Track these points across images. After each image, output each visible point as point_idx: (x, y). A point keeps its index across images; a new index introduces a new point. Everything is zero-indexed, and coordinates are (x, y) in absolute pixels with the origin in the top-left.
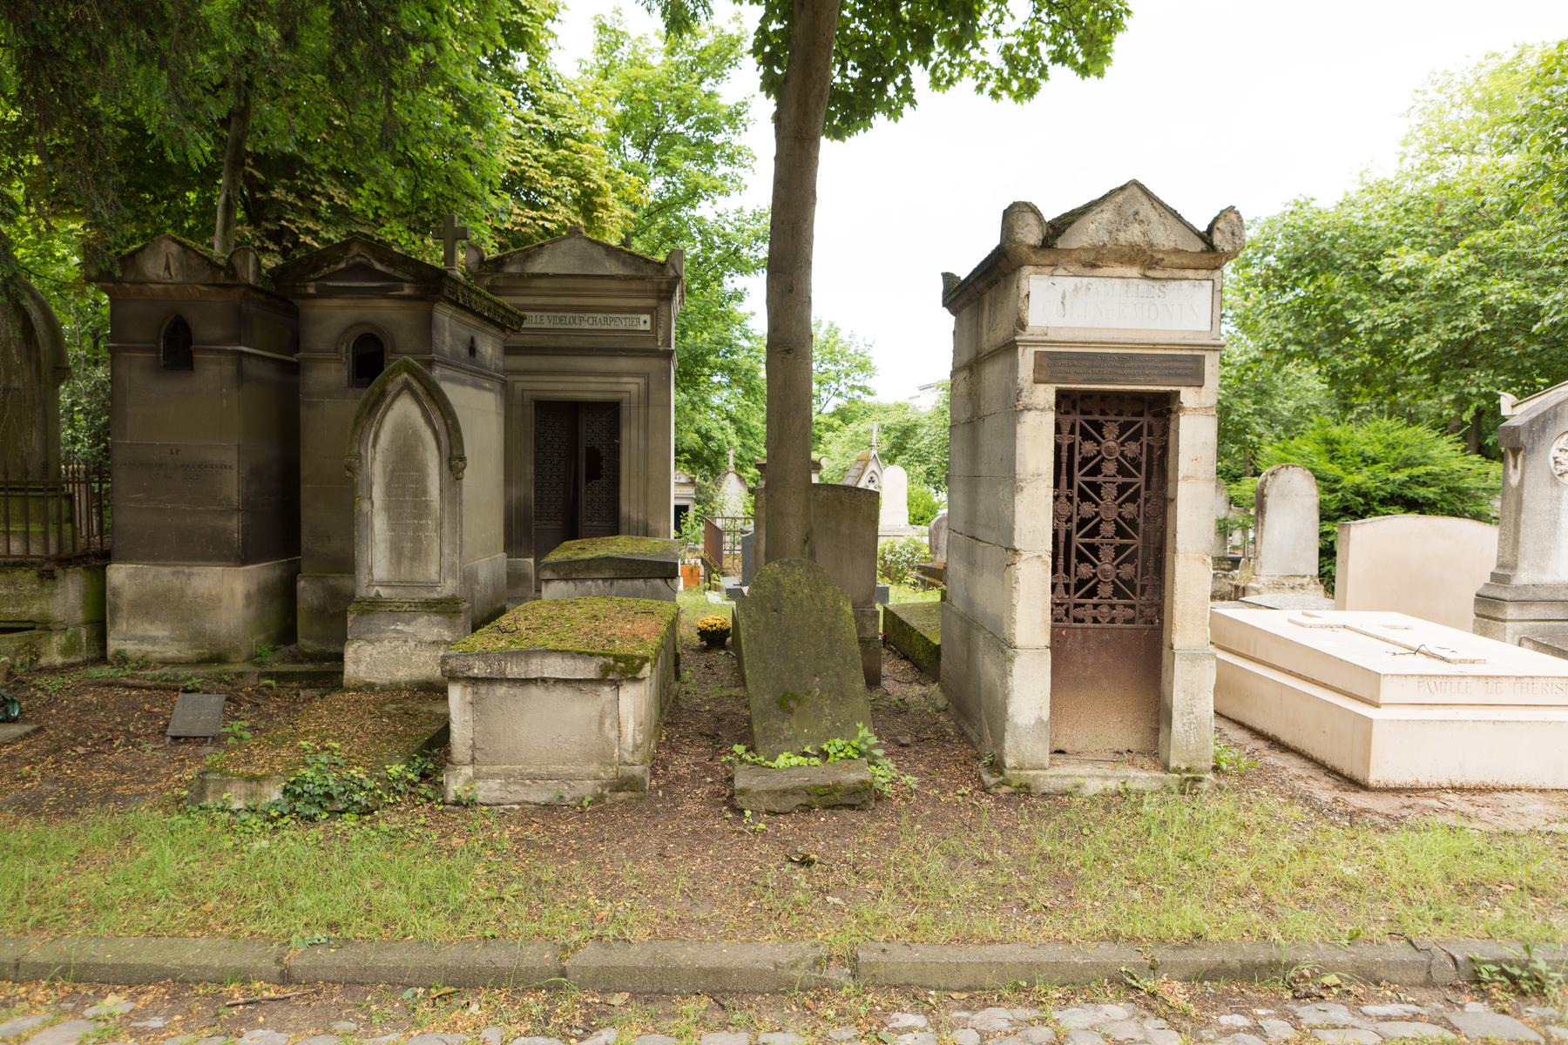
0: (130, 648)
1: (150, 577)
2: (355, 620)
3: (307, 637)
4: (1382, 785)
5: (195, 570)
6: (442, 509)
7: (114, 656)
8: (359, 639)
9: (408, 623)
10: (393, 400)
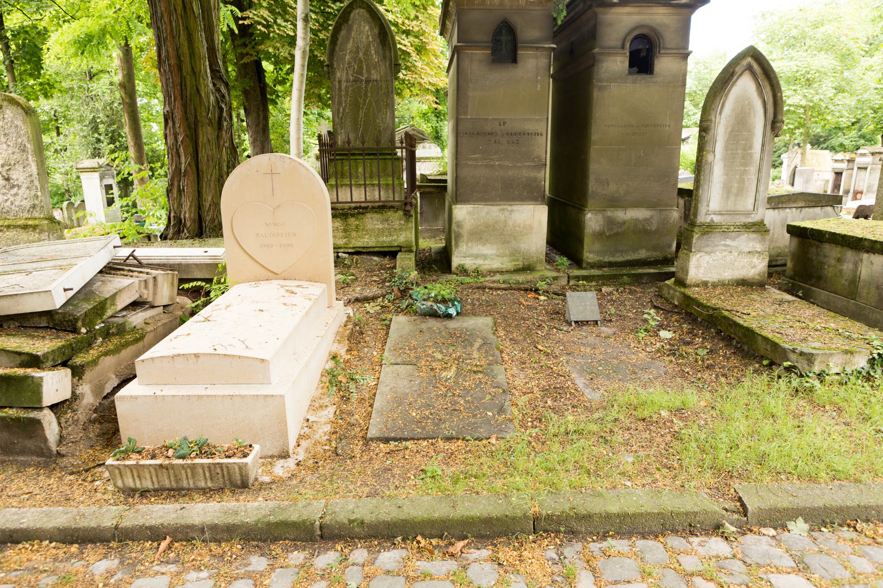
0: (469, 263)
1: (483, 214)
2: (698, 239)
3: (590, 252)
5: (515, 208)
6: (761, 159)
8: (699, 251)
9: (734, 239)
10: (738, 78)
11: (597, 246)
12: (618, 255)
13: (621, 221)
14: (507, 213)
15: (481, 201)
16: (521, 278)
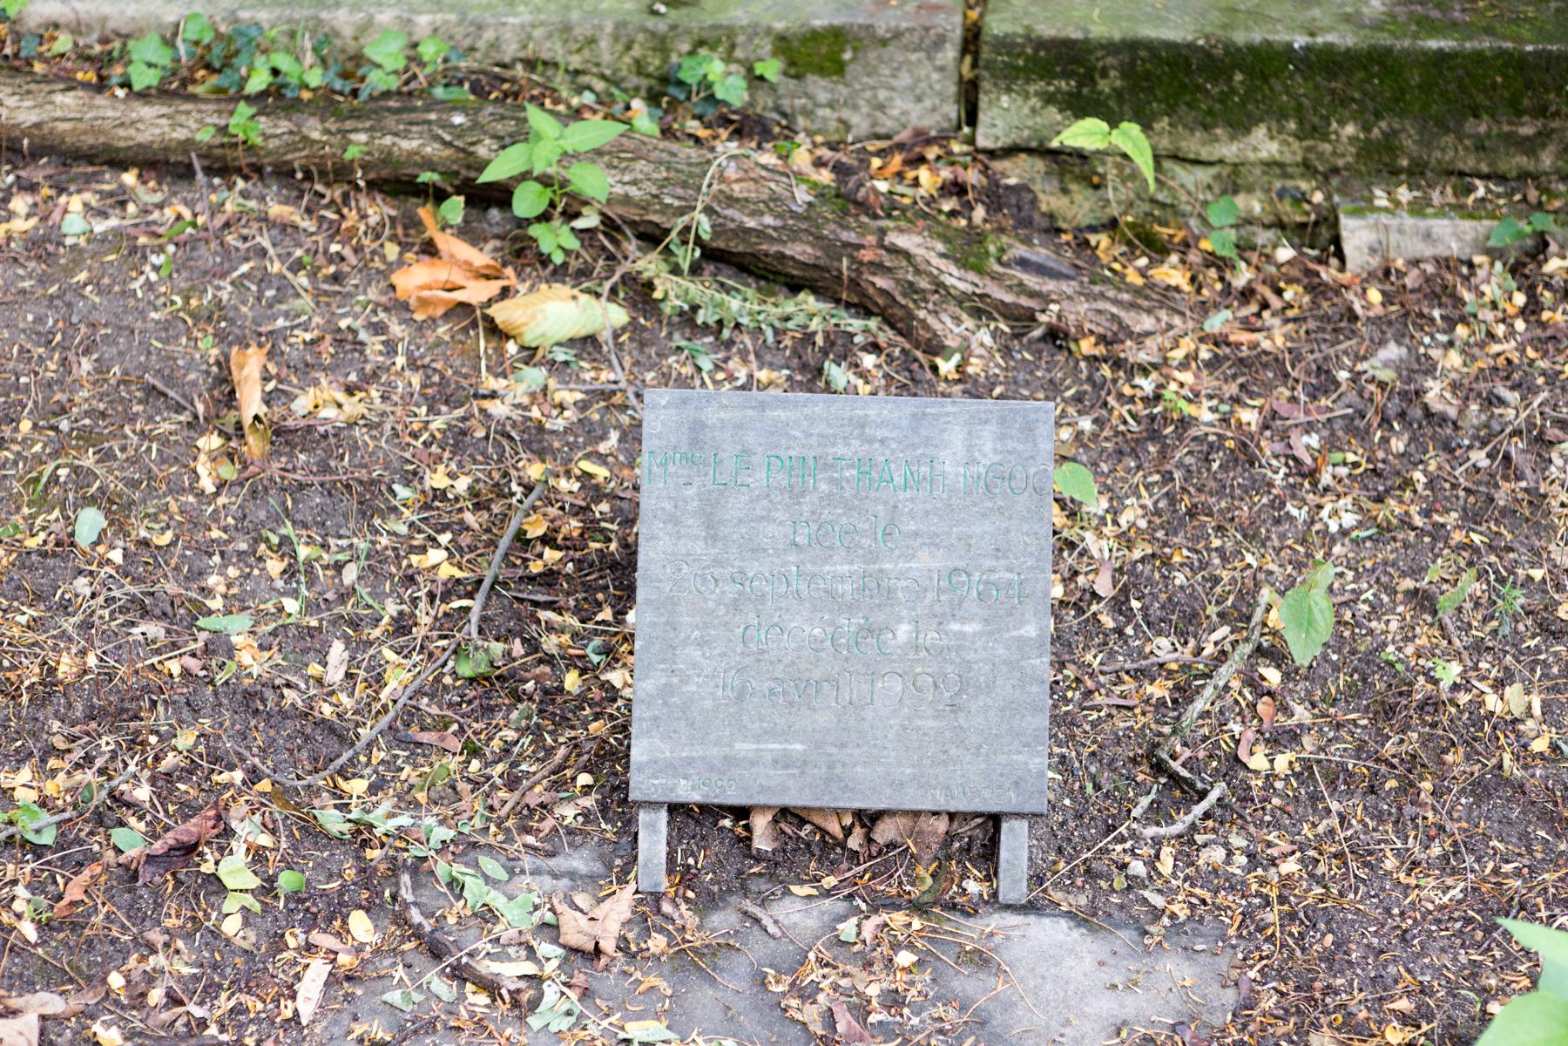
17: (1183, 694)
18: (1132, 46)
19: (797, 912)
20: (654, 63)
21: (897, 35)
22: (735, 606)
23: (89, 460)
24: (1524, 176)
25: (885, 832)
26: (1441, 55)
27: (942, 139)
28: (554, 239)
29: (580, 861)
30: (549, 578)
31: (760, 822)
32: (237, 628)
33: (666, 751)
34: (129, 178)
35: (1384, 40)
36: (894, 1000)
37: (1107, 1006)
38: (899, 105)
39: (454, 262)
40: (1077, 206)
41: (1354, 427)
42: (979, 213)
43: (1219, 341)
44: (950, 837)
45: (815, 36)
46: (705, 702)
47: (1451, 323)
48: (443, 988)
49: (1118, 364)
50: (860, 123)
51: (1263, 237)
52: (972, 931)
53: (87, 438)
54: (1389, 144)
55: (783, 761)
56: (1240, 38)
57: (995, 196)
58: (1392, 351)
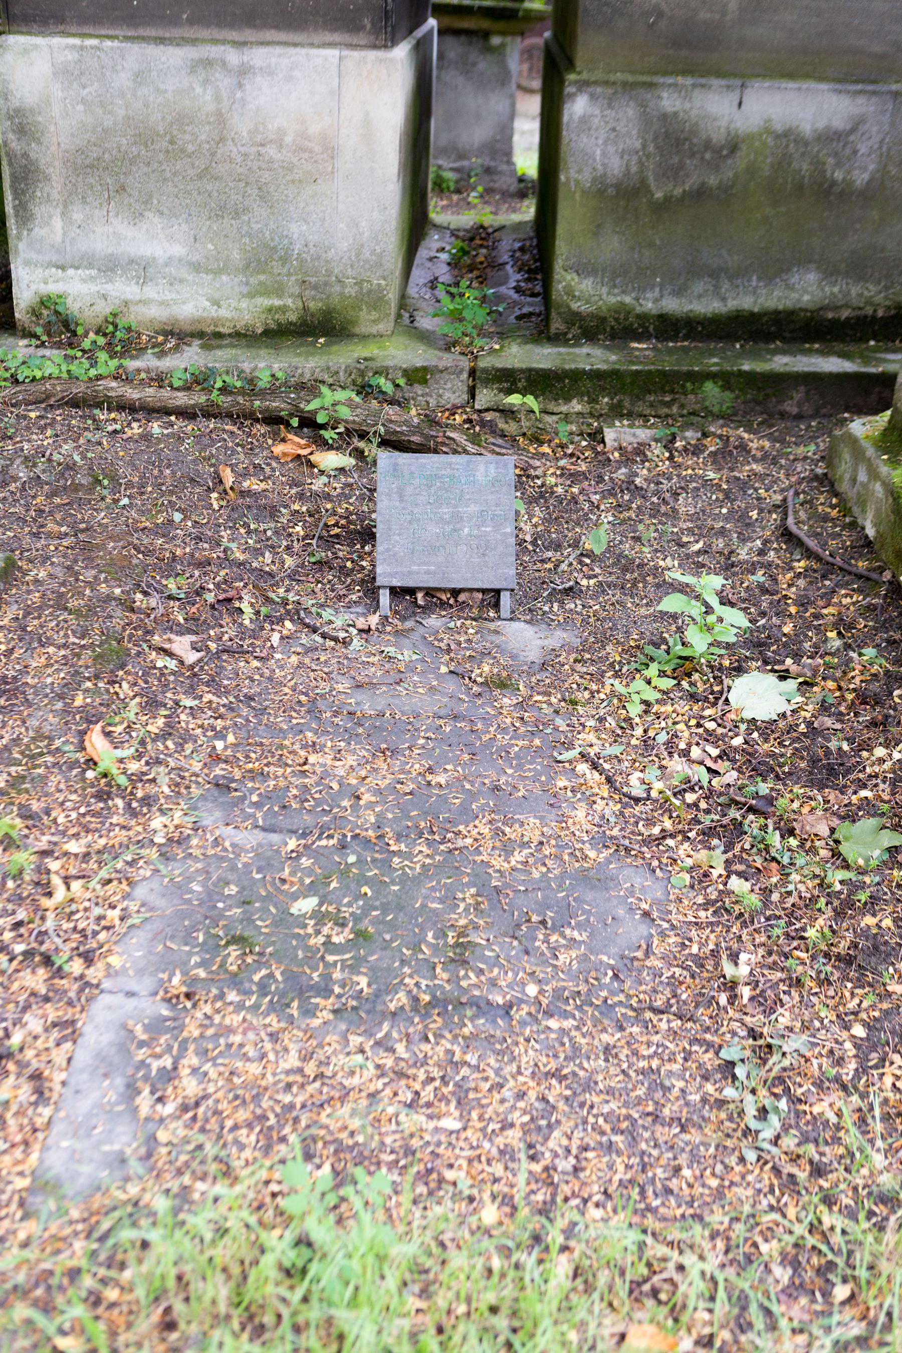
1: (123, 79)
3: (582, 270)
4: (463, 38)
5: (258, 56)
7: (35, 313)
11: (612, 246)
12: (699, 287)
13: (718, 137)
14: (225, 82)
15: (114, 22)
16: (267, 366)
17: (556, 566)
18: (530, 370)
19: (433, 621)
20: (359, 380)
21: (446, 369)
22: (410, 522)
23: (174, 498)
24: (667, 416)
25: (462, 597)
26: (637, 372)
27: (462, 407)
28: (329, 435)
29: (360, 609)
30: (337, 536)
31: (420, 596)
32: (234, 546)
33: (389, 570)
34: (173, 418)
35: (617, 367)
36: (469, 641)
37: (540, 643)
38: (447, 395)
39: (294, 443)
40: (511, 428)
41: (611, 493)
42: (477, 428)
43: (563, 468)
44: (483, 600)
45: (417, 370)
46: (396, 561)
47: (643, 462)
48: (319, 639)
49: (528, 477)
50: (433, 402)
51: (577, 439)
52: (492, 626)
53: (172, 493)
54: (620, 405)
55: (428, 573)
56: (567, 367)
57: (483, 424)
58: (623, 470)
